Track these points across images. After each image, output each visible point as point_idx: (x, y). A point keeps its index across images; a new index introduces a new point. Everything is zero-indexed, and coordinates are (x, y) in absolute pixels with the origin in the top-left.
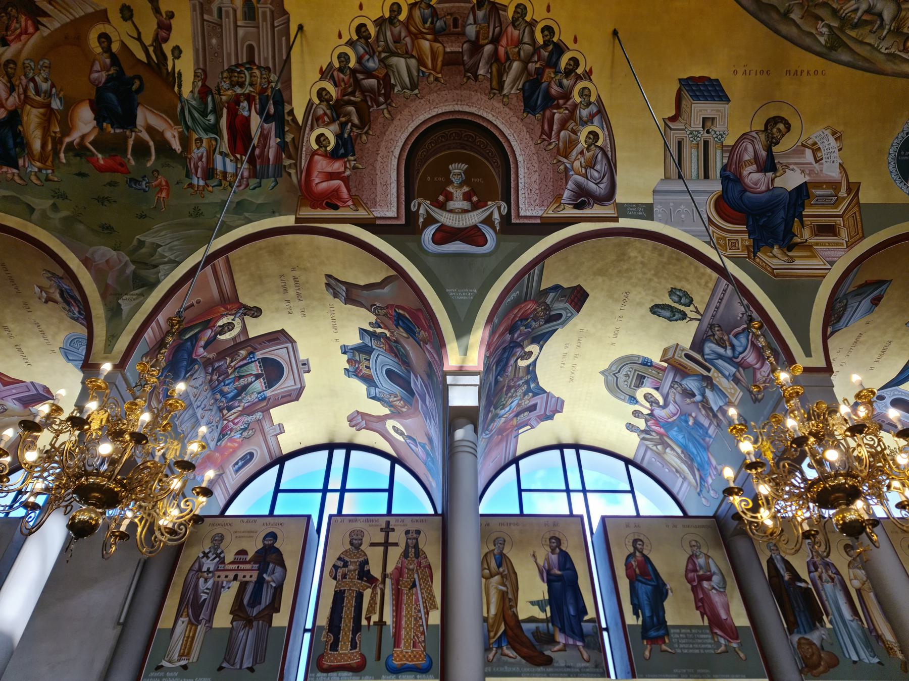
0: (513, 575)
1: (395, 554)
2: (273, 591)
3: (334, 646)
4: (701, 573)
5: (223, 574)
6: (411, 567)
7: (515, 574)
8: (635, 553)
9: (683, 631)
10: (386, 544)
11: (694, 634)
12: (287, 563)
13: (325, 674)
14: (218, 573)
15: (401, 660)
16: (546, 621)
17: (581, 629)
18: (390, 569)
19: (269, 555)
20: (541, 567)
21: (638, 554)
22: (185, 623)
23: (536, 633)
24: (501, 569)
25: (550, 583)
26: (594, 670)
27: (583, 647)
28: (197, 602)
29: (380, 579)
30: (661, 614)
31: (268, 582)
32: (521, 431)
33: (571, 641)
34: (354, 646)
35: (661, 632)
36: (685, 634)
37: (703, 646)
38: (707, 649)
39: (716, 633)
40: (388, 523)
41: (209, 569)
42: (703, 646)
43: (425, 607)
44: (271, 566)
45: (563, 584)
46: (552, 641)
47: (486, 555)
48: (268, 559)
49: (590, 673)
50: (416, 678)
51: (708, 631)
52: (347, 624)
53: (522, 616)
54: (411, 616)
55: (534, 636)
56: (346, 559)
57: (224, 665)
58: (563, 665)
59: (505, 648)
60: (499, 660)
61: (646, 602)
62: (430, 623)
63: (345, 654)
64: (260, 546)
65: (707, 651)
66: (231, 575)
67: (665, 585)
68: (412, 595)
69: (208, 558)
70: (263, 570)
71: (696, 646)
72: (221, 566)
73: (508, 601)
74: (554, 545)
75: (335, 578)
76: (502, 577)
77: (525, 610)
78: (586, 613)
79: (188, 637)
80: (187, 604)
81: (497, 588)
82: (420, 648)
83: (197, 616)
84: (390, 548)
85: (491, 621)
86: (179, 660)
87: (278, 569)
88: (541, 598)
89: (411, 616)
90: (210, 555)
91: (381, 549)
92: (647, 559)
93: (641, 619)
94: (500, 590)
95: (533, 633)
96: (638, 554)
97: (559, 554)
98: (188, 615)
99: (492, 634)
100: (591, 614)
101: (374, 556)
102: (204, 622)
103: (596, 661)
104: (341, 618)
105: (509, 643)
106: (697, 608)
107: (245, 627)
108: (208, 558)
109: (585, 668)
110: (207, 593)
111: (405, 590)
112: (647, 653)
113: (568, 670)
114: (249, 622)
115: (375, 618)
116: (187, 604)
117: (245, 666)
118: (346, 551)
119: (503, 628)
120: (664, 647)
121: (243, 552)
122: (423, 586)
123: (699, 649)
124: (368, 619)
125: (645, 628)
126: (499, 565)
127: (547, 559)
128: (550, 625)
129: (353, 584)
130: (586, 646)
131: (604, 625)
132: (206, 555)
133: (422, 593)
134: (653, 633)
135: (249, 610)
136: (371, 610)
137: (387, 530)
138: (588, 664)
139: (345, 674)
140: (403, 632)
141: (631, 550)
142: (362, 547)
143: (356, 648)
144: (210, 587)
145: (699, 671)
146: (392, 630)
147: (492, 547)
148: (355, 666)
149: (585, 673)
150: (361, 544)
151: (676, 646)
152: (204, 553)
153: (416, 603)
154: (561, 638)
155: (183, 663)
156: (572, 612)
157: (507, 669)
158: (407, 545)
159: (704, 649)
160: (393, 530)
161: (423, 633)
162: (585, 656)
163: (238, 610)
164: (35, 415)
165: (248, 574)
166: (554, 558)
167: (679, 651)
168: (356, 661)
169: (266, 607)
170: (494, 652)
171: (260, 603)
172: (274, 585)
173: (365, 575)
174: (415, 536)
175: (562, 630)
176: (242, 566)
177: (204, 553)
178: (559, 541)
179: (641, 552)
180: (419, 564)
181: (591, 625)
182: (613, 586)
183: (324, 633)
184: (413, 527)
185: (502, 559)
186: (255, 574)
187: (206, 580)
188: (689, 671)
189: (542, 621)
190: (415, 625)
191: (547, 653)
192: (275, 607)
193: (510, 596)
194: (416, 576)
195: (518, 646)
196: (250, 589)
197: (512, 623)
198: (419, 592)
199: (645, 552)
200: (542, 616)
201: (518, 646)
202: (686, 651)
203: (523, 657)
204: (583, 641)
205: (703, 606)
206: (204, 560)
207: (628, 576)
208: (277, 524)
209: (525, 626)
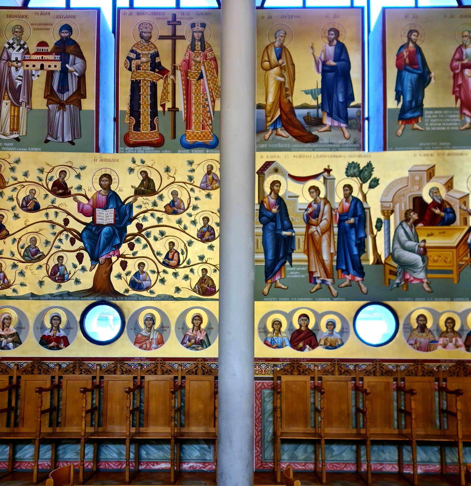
0: (291, 67)
1: (182, 47)
2: (77, 80)
3: (137, 127)
4: (466, 61)
5: (31, 64)
6: (198, 59)
7: (293, 65)
8: (408, 43)
9: (436, 112)
10: (174, 37)
11: (445, 115)
12: (85, 55)
13: (132, 148)
14: (26, 63)
15: (193, 139)
16: (317, 107)
17: (347, 114)
18: (179, 61)
19: (67, 47)
20: (318, 59)
21: (411, 45)
22: (9, 105)
23: (307, 118)
24: (280, 61)
25: (324, 73)
26: (353, 145)
27: (346, 128)
28: (14, 88)
29: (170, 70)
30: (420, 98)
31: (71, 72)
32: (358, 178)
33: (336, 123)
34: (153, 127)
35: (416, 114)
36: (437, 114)
37: (450, 124)
38: (453, 126)
39: (465, 114)
40: (174, 16)
41: (17, 59)
42: (450, 124)
43: (212, 96)
44: (71, 57)
45: (336, 76)
46: (319, 122)
47: (267, 47)
48: (67, 51)
49: (349, 147)
50: (205, 152)
51: (458, 112)
52: (145, 110)
53: (295, 104)
54: (200, 104)
55: (305, 120)
56: (139, 51)
57: (49, 138)
58: (326, 141)
59: (279, 130)
60: (274, 139)
61: (409, 89)
62: (215, 110)
63: (146, 133)
64: (58, 38)
65: (453, 128)
66: (38, 65)
67: (429, 73)
68: (200, 85)
69: (14, 48)
70: (64, 61)
71: (444, 124)
72: (27, 57)
73: (284, 90)
74: (333, 37)
75: (130, 69)
76: (281, 68)
77: (299, 98)
78: (353, 100)
79: (14, 116)
80: (6, 89)
81: (275, 79)
82: (208, 130)
83: (16, 98)
84: (178, 41)
85: (268, 108)
86: (12, 134)
87: (79, 61)
88: (314, 87)
89: (200, 104)
90: (15, 45)
91: (169, 42)
92: (418, 50)
93: (401, 103)
94: (278, 81)
95: (304, 118)
96: (411, 45)
97: (336, 46)
98: (9, 98)
99: (269, 119)
100: (358, 100)
101: (164, 47)
102: (24, 104)
103: (355, 139)
104: (140, 104)
105: (283, 126)
106: (454, 93)
107: (59, 109)
108: (14, 48)
109: (345, 144)
110: (21, 80)
111: (193, 81)
112: (400, 131)
113: (331, 145)
114: (62, 105)
115: (169, 105)
116: (6, 89)
117: (66, 140)
118: (137, 44)
119: (278, 113)
120: (416, 126)
121: (43, 44)
122: (209, 78)
123: (446, 126)
124: (163, 106)
125: (403, 111)
126: (279, 58)
127: (324, 51)
128: (320, 110)
129: (147, 76)
130: (349, 127)
131: (366, 116)
132: (11, 46)
133: (209, 84)
134: (409, 115)
135: (60, 95)
136: (165, 93)
137: (174, 22)
138: (348, 141)
139: (149, 148)
140: (193, 117)
141: (405, 40)
142: (152, 40)
143: (155, 129)
144: (22, 75)
145: (441, 144)
146: (184, 116)
147: (273, 40)
148: (156, 143)
149: (345, 147)
150: (150, 37)
151: (427, 124)
152: (9, 44)
153: (203, 92)
154: (327, 121)
155: (16, 136)
156: (341, 99)
157: (280, 145)
158: (193, 39)
159: (450, 127)
160: (180, 23)
161: (210, 118)
162: (347, 135)
163: (50, 95)
164: (16, 317)
165: (53, 64)
166: (331, 50)
167: (428, 129)
168: (155, 138)
169: (74, 94)
170: (270, 132)
171: (68, 90)
172: (77, 74)
173: (156, 66)
174: (200, 29)
175: (330, 115)
176: (46, 57)
177: (9, 44)
178: (337, 33)
179: (414, 43)
180: (205, 57)
181: (356, 110)
182: (382, 75)
183: (127, 116)
184: (198, 20)
185: (282, 52)
186: (59, 64)
187: (17, 68)
188: (433, 144)
189: (313, 107)
190: (203, 111)
191: (314, 133)
192: (81, 93)
193: (287, 86)
194: (203, 68)
195: (291, 128)
196: (57, 77)
197: (287, 109)
198: (206, 83)
199: (418, 43)
200: (314, 103)
201: (291, 128)
202: (434, 129)
203: (294, 137)
204: (346, 122)
205: (460, 91)
206: (10, 50)
207: (397, 66)
208: (70, 17)
209: (297, 112)
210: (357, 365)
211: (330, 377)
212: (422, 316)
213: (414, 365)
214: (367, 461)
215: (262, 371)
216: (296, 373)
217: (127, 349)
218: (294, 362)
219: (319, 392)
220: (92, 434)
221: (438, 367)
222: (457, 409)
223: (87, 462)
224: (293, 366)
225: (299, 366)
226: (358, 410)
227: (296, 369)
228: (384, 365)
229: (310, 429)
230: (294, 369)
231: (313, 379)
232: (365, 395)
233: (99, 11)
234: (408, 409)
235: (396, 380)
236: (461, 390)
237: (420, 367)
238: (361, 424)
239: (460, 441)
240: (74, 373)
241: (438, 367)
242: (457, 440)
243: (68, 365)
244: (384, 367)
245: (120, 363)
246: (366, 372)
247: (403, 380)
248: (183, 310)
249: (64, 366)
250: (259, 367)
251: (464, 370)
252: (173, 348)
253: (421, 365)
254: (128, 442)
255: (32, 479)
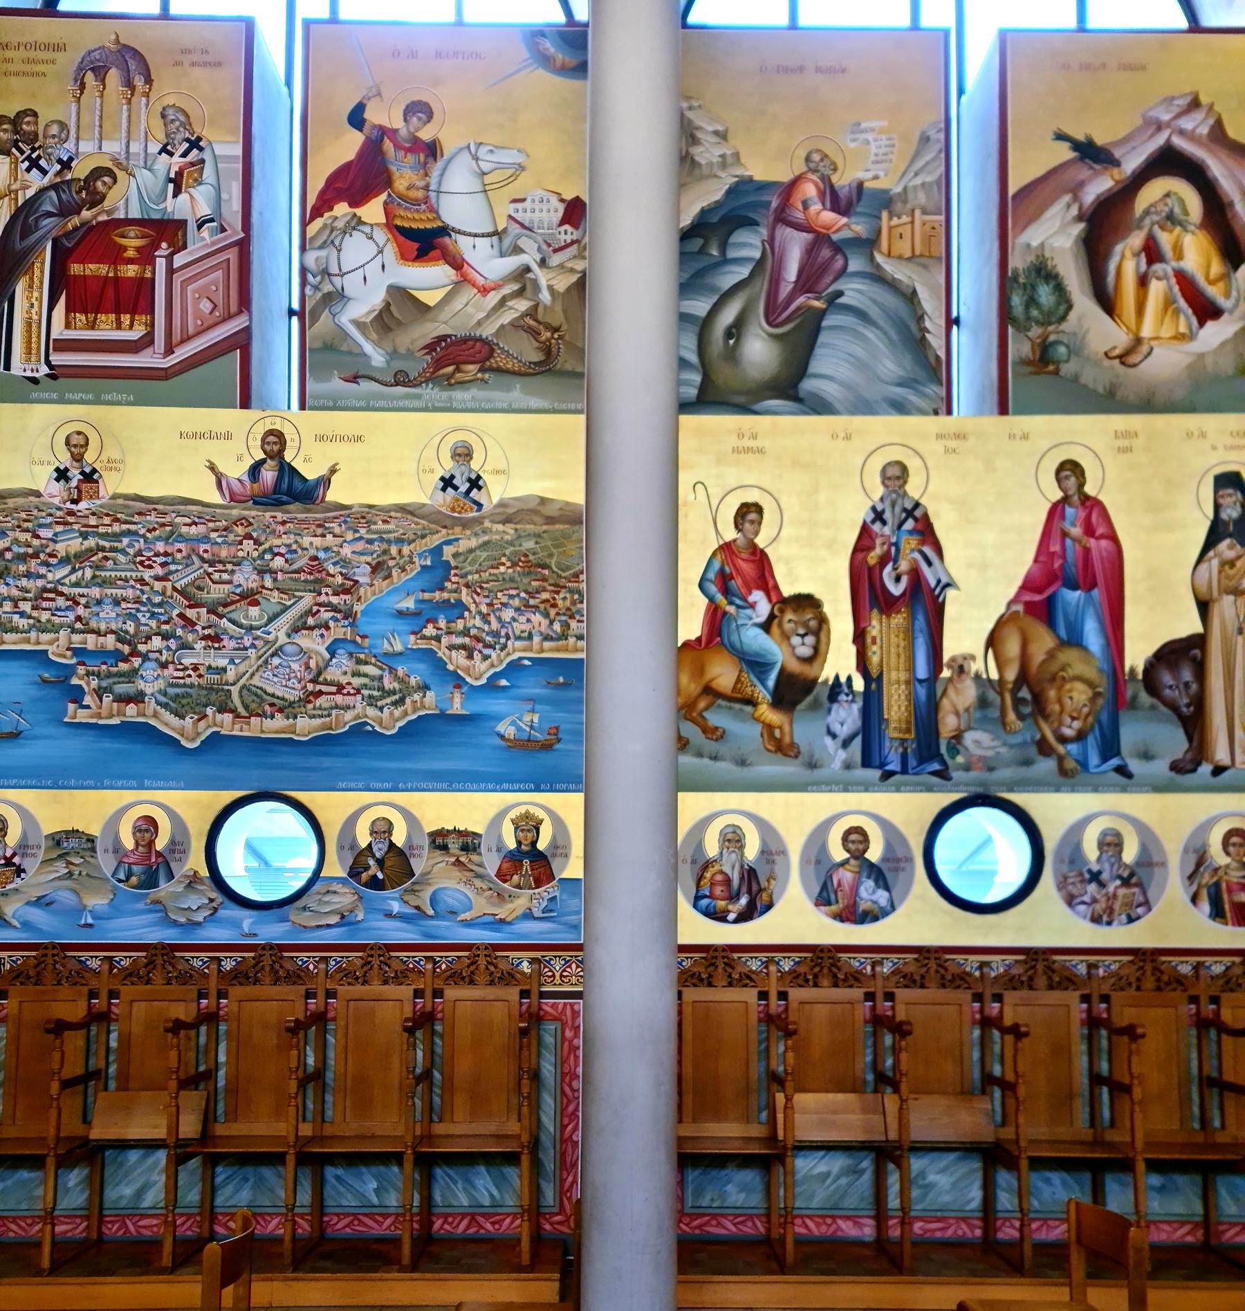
210: (1198, 963)
211: (915, 994)
212: (859, 830)
213: (1025, 962)
214: (1021, 1210)
215: (554, 976)
216: (825, 982)
217: (1052, 924)
218: (927, 955)
219: (779, 1029)
220: (311, 1140)
221: (1091, 966)
222: (1131, 1074)
223: (182, 1215)
224: (713, 964)
225: (835, 964)
226: (1096, 1080)
227: (826, 971)
228: (947, 960)
229: (756, 1131)
230: (1143, 974)
231: (763, 995)
232: (898, 1037)
233: (249, 26)
234: (1010, 1077)
235: (1086, 998)
236: (909, 1023)
237: (1040, 966)
238: (1106, 1114)
239: (1139, 1158)
240: (365, 982)
241: (982, 965)
242: (1131, 1155)
243: (1228, 968)
244: (1163, 967)
245: (1039, 965)
246: (1228, 982)
247: (890, 996)
248: (351, 811)
249: (228, 965)
250: (578, 967)
251: (1153, 975)
252: (795, 919)
253: (1153, 961)
254: (291, 1160)
255: (519, 1256)
